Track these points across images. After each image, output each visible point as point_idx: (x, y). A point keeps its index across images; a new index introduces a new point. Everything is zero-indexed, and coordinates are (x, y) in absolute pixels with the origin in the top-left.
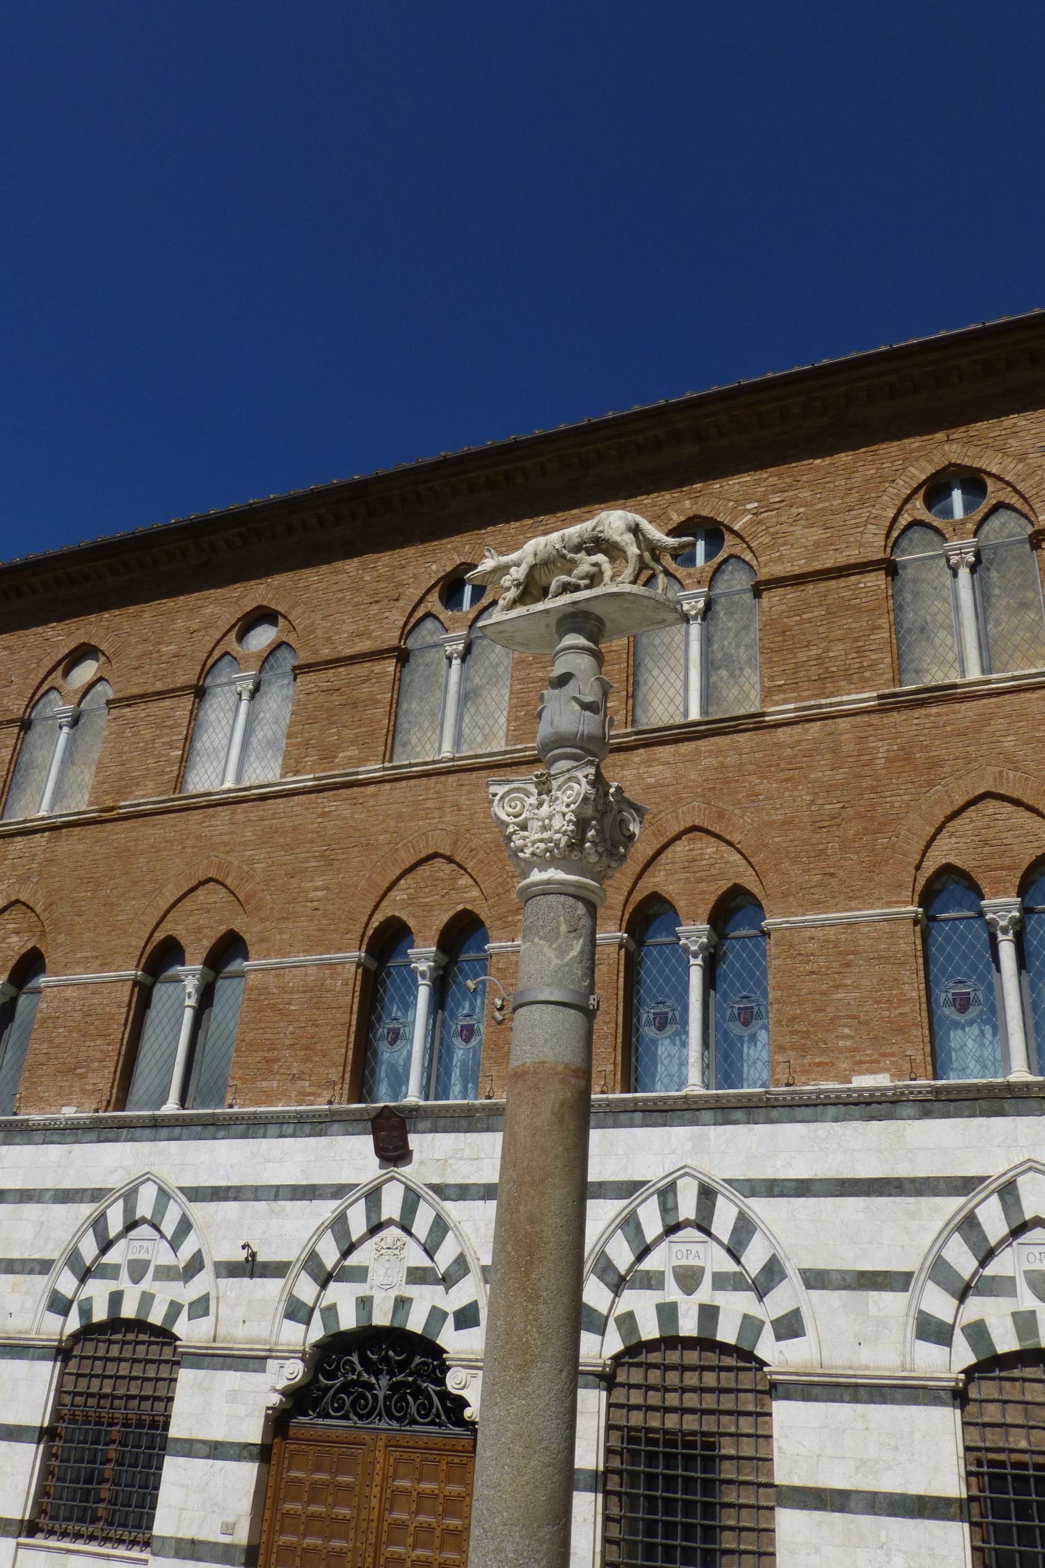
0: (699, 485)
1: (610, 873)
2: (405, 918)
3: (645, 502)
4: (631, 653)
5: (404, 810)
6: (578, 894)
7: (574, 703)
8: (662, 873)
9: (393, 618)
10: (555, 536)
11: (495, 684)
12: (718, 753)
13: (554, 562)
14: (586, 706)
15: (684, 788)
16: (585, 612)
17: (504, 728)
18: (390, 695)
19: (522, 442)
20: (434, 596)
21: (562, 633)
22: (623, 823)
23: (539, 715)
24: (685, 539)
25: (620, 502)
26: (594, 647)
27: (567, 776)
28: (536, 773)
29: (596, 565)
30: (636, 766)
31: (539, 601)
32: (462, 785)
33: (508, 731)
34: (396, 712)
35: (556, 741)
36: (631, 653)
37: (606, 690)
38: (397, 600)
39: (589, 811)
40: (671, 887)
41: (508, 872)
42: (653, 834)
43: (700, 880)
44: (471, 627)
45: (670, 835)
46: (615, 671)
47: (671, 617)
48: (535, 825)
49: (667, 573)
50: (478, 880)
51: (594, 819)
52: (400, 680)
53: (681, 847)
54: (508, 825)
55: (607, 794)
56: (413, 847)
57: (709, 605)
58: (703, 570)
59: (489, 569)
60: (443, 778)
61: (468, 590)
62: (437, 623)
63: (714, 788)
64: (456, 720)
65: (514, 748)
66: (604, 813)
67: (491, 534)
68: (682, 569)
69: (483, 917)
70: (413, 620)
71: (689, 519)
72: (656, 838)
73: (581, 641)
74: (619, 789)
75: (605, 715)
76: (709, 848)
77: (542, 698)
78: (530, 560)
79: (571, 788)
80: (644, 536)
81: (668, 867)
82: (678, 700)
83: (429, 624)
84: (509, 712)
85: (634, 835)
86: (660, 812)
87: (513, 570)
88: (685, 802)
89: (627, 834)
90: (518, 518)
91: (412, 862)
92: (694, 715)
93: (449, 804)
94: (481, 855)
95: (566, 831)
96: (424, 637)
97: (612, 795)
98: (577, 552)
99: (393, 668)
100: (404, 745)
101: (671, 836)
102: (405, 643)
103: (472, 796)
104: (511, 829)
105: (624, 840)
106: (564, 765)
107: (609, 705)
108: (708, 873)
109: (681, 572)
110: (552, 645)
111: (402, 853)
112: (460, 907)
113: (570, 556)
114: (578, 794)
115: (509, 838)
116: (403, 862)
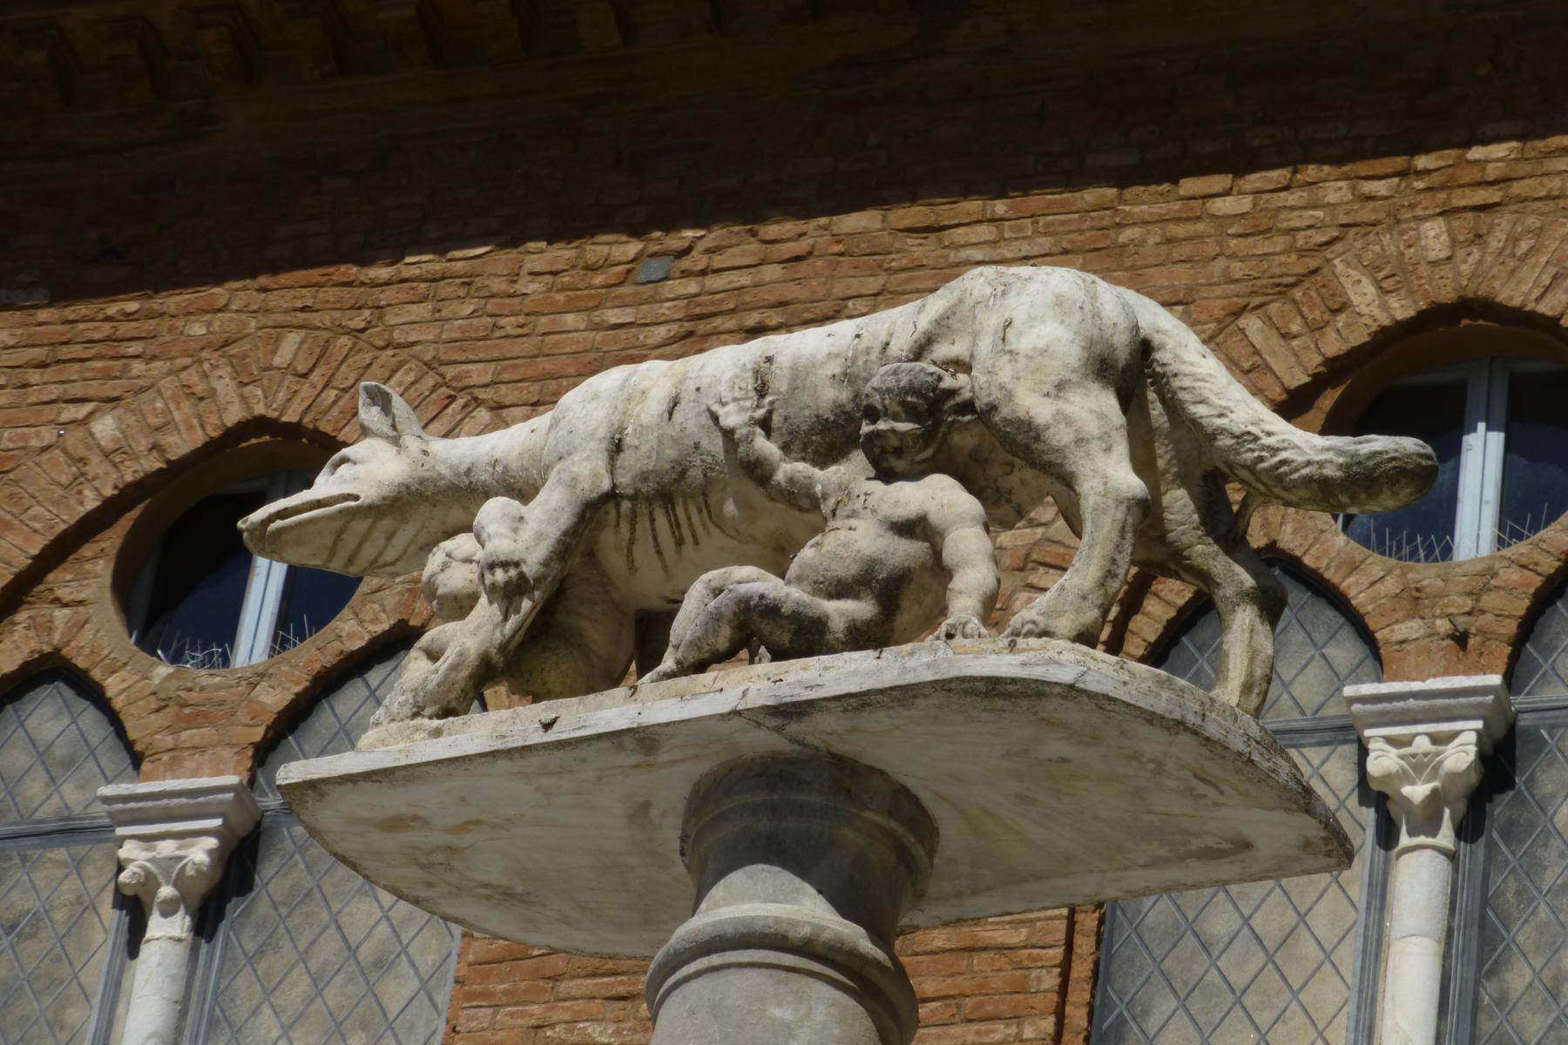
0: (1500, 150)
3: (1222, 206)
4: (1081, 970)
10: (724, 365)
13: (704, 494)
16: (839, 761)
20: (91, 578)
24: (1378, 443)
25: (1090, 195)
26: (866, 945)
29: (914, 528)
31: (613, 679)
36: (1081, 970)
44: (265, 752)
47: (1274, 830)
57: (1501, 760)
59: (368, 493)
61: (265, 584)
62: (90, 718)
67: (426, 295)
68: (1376, 564)
71: (1435, 317)
73: (805, 908)
78: (587, 470)
80: (1174, 407)
87: (494, 512)
98: (826, 455)
109: (1371, 580)
110: (658, 911)
113: (790, 469)
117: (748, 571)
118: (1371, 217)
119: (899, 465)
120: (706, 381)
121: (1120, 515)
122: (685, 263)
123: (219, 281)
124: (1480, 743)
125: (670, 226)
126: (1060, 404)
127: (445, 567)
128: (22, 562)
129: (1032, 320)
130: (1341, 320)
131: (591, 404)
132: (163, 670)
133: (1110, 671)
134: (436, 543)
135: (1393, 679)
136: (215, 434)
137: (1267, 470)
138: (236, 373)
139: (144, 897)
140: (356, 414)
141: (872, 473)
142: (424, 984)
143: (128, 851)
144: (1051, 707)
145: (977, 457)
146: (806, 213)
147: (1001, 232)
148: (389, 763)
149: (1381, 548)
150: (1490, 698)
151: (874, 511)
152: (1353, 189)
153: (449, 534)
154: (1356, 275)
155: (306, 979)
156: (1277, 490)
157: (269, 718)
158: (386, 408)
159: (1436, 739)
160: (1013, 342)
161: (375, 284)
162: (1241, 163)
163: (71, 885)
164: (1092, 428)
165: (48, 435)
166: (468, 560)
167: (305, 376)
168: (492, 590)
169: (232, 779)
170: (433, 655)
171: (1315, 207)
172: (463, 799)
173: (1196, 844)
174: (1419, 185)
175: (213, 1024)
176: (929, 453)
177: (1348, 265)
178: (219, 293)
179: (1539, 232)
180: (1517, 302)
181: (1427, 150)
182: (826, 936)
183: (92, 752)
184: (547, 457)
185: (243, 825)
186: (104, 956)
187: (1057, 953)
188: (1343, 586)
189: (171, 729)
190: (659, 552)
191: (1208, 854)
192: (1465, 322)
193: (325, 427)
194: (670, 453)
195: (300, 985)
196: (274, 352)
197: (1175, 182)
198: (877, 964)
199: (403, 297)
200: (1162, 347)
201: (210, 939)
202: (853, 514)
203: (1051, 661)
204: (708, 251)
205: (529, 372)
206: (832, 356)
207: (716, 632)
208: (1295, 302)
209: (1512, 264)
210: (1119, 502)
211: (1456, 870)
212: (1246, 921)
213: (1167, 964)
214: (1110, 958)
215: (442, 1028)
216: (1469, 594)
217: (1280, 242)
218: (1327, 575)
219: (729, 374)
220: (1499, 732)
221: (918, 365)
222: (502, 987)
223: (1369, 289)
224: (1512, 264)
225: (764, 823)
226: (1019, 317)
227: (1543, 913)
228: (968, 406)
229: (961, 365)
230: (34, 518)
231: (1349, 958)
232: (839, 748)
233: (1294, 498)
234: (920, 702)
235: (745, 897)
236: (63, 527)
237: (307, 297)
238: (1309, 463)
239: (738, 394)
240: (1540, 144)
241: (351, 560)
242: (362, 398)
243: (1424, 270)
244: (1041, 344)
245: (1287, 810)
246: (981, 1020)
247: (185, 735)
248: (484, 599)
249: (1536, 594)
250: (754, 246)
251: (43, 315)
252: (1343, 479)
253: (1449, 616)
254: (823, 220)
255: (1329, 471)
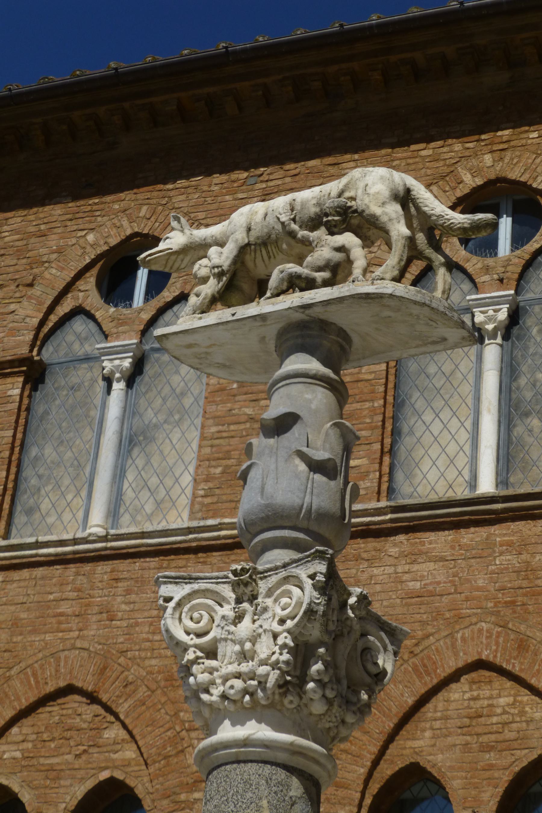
0: (507, 132)
1: (344, 732)
2: (16, 788)
3: (424, 153)
4: (391, 385)
5: (23, 615)
6: (293, 765)
7: (297, 460)
8: (428, 734)
9: (22, 312)
10: (280, 203)
11: (178, 423)
12: (523, 546)
13: (276, 242)
14: (316, 467)
15: (467, 599)
17: (189, 491)
18: (10, 433)
19: (235, 52)
20: (89, 283)
21: (284, 354)
22: (367, 653)
23: (244, 476)
25: (383, 152)
27: (283, 574)
28: (234, 567)
29: (341, 249)
30: (391, 561)
32: (117, 580)
33: (195, 496)
34: (19, 460)
35: (265, 519)
36: (391, 385)
37: (349, 443)
38: (31, 285)
39: (315, 632)
40: (440, 757)
41: (183, 722)
42: (415, 669)
43: (487, 748)
44: (144, 332)
45: (443, 672)
46: (365, 412)
47: (453, 334)
48: (228, 650)
49: (452, 266)
50: (135, 732)
51: (322, 644)
52: (28, 409)
53: (457, 693)
54: (186, 649)
55: (344, 605)
56: (35, 675)
57: (515, 316)
58: (508, 262)
59: (175, 247)
60: (87, 567)
61: (142, 275)
62: (92, 325)
63: (513, 603)
64: (114, 476)
65: (202, 523)
66: (338, 636)
67: (183, 192)
68: (475, 259)
69: (140, 791)
70: (54, 318)
71: (489, 183)
72: (420, 676)
73: (314, 365)
74: (363, 599)
75: (346, 483)
76: (502, 697)
77: (249, 450)
78: (241, 237)
79: (288, 594)
80: (418, 208)
81: (437, 724)
82: (462, 461)
83: (79, 325)
84: (198, 467)
85: (384, 672)
86: (427, 636)
87: (213, 251)
88: (467, 622)
89: (373, 670)
90: (225, 169)
91: (32, 699)
92: (487, 485)
93: (96, 609)
94: (142, 692)
95: (277, 662)
96: (70, 345)
97: (352, 607)
99: (17, 391)
100: (29, 512)
101: (443, 675)
102: (39, 354)
103: (133, 597)
104: (190, 655)
105: (368, 680)
106: (278, 556)
107: (352, 463)
108: (500, 737)
109: (474, 264)
111: (16, 683)
112: (104, 775)
113: (302, 233)
114: (299, 604)
115: (187, 670)
116: (18, 699)
117: (291, 265)
118: (469, 154)
119: (336, 230)
120: (275, 208)
121: (403, 242)
122: (261, 178)
123: (122, 191)
124: (508, 311)
125: (256, 167)
126: (384, 209)
127: (199, 269)
128: (69, 279)
129: (374, 184)
130: (461, 186)
131: (241, 216)
132: (112, 309)
133: (402, 289)
134: (196, 261)
135: (481, 293)
136: (123, 238)
137: (447, 226)
138: (128, 219)
139: (111, 377)
140: (170, 224)
141: (327, 233)
142: (196, 399)
143: (105, 364)
144: (385, 301)
145: (359, 227)
146: (297, 161)
147: (357, 164)
148: (187, 328)
149: (476, 254)
150: (511, 298)
151: (329, 245)
152: (463, 146)
153: (200, 259)
154: (465, 172)
155: (160, 399)
156: (450, 232)
157: (145, 322)
158: (179, 221)
159: (495, 311)
160: (369, 191)
161: (168, 190)
162: (429, 140)
163: (89, 375)
164: (394, 215)
165: (74, 241)
166: (206, 266)
167: (149, 219)
168: (214, 275)
169: (135, 341)
170: (198, 295)
171: (452, 152)
172: (209, 338)
173: (430, 340)
174: (483, 144)
175: (134, 414)
176: (344, 226)
177: (462, 169)
178: (122, 195)
179: (520, 157)
180: (514, 178)
181: (485, 133)
182: (320, 373)
183: (93, 335)
184: (228, 234)
185: (139, 355)
186: (100, 395)
187: (384, 381)
188: (465, 266)
189: (116, 327)
190: (264, 261)
191: (434, 343)
192: (499, 185)
193: (156, 234)
194: (266, 230)
195: (159, 401)
196: (140, 212)
197: (409, 146)
198: (336, 380)
199: (177, 193)
200: (413, 190)
201: (131, 388)
202: (322, 246)
203: (384, 287)
204: (268, 174)
205: (217, 214)
206: (313, 198)
207: (282, 284)
208: (447, 181)
209: (512, 166)
210: (403, 238)
211: (502, 350)
212: (440, 368)
213: (417, 382)
214: (399, 381)
215: (202, 411)
216: (503, 267)
217: (442, 163)
218: (460, 263)
219: (282, 205)
220: (514, 308)
221: (340, 199)
222: (219, 399)
223: (469, 175)
224: (512, 166)
225: (300, 341)
226: (370, 183)
227: (530, 361)
228: (356, 211)
229: (353, 199)
230: (71, 266)
231: (471, 378)
232: (322, 317)
233: (455, 234)
234: (345, 302)
235: (295, 363)
236: (80, 268)
237: (149, 195)
238: (459, 223)
239: (285, 211)
240: (519, 130)
241: (171, 268)
242: (172, 219)
243: (485, 169)
244: (377, 191)
245: (457, 328)
246: (361, 402)
247: (120, 328)
248: (212, 278)
249: (523, 266)
250: (282, 172)
251: (70, 205)
252: (470, 228)
253: (497, 274)
254: (303, 163)
255: (466, 225)
